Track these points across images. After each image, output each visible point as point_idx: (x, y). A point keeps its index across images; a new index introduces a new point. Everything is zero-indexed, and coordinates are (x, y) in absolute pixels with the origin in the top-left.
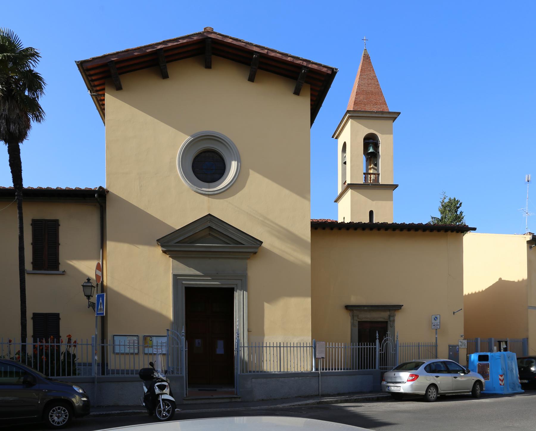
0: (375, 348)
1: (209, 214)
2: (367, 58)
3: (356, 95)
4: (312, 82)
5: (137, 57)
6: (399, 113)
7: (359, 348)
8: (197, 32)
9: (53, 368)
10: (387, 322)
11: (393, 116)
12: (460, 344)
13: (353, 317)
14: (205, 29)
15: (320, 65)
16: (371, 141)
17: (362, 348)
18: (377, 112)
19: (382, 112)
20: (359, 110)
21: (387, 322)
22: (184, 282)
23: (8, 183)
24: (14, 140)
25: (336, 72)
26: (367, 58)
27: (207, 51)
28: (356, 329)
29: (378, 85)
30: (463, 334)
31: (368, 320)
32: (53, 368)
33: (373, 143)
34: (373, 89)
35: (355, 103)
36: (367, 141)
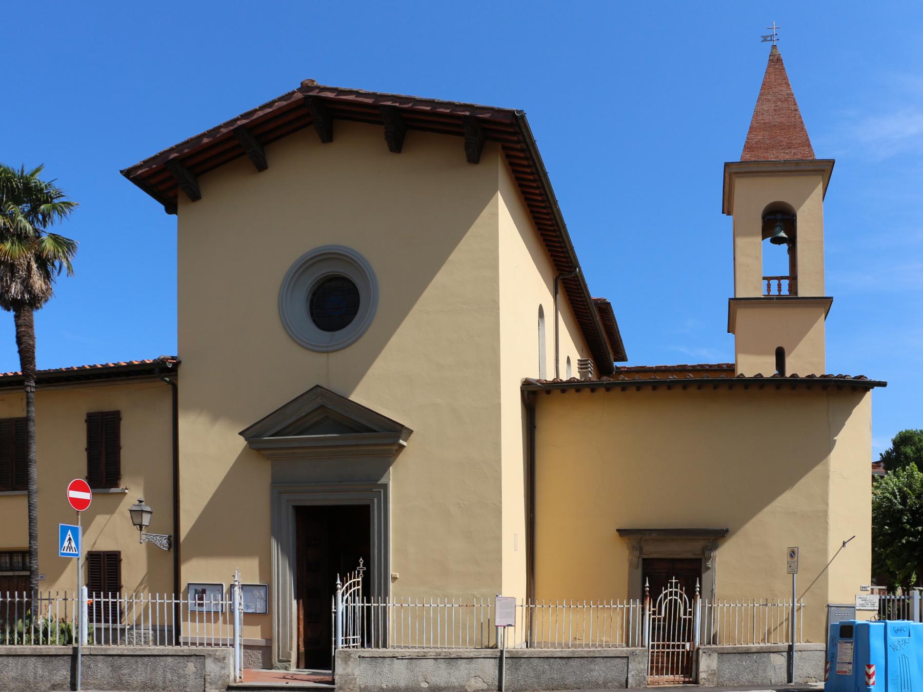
0: (91, 620)
1: (317, 386)
2: (776, 61)
3: (750, 132)
5: (210, 147)
8: (371, 91)
10: (701, 560)
12: (859, 602)
13: (632, 548)
14: (302, 83)
15: (357, 93)
16: (779, 216)
18: (786, 162)
19: (797, 163)
20: (753, 159)
21: (701, 560)
22: (376, 500)
23: (11, 365)
24: (24, 306)
26: (776, 61)
27: (316, 116)
29: (796, 110)
31: (662, 556)
35: (748, 147)
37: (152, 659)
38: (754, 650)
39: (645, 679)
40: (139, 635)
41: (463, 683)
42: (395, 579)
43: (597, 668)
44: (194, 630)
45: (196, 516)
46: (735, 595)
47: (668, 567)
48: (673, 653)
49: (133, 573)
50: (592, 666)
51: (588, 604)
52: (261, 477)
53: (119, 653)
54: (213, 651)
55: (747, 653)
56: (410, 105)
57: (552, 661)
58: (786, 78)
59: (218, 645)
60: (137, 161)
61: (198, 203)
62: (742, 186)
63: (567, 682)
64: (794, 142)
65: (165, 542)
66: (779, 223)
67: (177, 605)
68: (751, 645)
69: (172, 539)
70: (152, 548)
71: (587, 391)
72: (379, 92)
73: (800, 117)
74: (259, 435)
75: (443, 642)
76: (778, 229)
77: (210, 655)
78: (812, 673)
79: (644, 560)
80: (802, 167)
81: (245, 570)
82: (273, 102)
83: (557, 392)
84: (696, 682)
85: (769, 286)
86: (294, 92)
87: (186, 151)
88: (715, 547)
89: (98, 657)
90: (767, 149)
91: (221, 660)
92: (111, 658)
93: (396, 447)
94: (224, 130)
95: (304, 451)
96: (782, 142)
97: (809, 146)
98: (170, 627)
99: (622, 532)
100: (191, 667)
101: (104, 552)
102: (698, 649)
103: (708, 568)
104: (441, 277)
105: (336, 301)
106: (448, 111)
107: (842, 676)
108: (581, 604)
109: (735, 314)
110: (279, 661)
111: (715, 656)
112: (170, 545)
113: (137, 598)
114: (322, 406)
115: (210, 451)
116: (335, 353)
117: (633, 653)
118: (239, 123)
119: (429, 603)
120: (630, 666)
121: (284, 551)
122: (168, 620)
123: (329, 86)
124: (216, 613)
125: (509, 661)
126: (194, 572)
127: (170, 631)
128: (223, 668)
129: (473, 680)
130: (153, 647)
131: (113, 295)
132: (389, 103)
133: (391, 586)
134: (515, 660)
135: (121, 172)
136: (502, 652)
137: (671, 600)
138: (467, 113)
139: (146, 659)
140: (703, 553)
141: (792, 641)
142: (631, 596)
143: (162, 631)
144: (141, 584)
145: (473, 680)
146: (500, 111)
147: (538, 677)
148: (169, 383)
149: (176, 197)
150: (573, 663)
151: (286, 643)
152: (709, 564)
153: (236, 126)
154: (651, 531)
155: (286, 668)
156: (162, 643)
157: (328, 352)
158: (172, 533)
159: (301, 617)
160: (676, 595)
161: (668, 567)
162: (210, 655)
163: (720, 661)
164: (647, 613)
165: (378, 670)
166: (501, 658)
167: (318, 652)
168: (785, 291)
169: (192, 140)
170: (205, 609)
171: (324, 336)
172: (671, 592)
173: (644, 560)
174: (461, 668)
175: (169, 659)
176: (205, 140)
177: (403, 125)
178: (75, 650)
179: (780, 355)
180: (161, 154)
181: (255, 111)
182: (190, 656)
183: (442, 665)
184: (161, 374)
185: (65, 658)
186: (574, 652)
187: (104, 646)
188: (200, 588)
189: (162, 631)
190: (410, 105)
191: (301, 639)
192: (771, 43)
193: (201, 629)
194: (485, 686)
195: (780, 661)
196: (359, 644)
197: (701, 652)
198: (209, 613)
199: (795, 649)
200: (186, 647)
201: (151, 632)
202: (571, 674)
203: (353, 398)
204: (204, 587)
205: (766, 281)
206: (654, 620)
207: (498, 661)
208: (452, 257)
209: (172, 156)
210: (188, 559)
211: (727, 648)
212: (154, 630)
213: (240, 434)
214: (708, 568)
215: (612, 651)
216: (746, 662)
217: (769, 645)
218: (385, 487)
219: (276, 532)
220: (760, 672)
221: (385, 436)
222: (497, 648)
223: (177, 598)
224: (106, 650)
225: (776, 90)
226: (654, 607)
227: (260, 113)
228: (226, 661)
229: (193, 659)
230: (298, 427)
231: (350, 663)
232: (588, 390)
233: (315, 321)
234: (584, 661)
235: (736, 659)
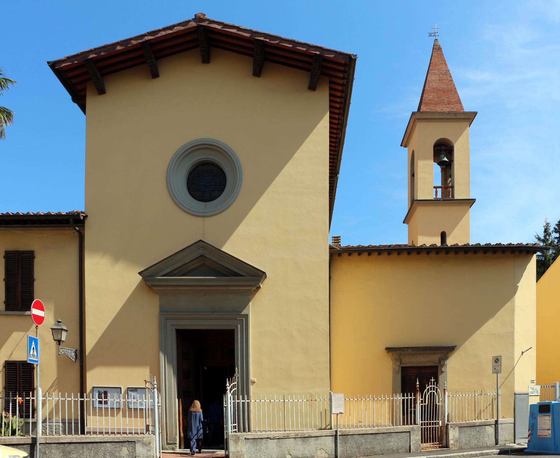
1: (201, 241)
2: (437, 49)
4: (328, 74)
5: (121, 53)
6: (475, 113)
7: (403, 400)
8: (248, 28)
9: (396, 420)
10: (437, 367)
11: (470, 117)
14: (195, 15)
15: (238, 28)
16: (443, 148)
17: (407, 400)
18: (449, 113)
19: (455, 114)
20: (428, 110)
21: (437, 367)
22: (239, 326)
25: (355, 60)
26: (437, 49)
27: (203, 42)
28: (399, 376)
29: (452, 81)
30: (534, 378)
32: (396, 420)
33: (445, 150)
34: (445, 86)
36: (439, 148)
37: (95, 445)
38: (478, 424)
39: (420, 446)
40: (51, 428)
41: (313, 454)
42: (253, 382)
43: (392, 440)
44: (107, 421)
45: (99, 335)
46: (458, 391)
47: (417, 373)
48: (433, 428)
49: (43, 380)
50: (390, 439)
51: (384, 397)
52: (151, 307)
53: (69, 441)
54: (141, 438)
55: (474, 426)
56: (277, 42)
57: (366, 436)
58: (444, 60)
59: (126, 433)
60: (62, 57)
61: (103, 97)
62: (420, 127)
63: (376, 450)
64: (451, 100)
65: (73, 354)
66: (443, 152)
67: (82, 402)
68: (477, 421)
69: (78, 352)
70: (61, 360)
71: (376, 254)
72: (255, 29)
73: (454, 85)
74: (153, 275)
75: (297, 427)
76: (443, 156)
77: (139, 441)
78: (508, 438)
79: (402, 367)
80: (458, 117)
81: (138, 376)
82: (174, 26)
83: (345, 255)
84: (447, 446)
85: (436, 192)
86: (189, 21)
87: (103, 54)
88: (446, 358)
89: (52, 445)
90: (436, 104)
91: (147, 444)
92: (62, 446)
93: (255, 288)
94: (134, 42)
95: (162, 288)
96: (444, 100)
97: (460, 103)
98: (76, 420)
99: (389, 350)
100: (125, 450)
101: (20, 362)
102: (447, 425)
103: (442, 372)
104: (288, 169)
105: (208, 179)
106: (305, 49)
107: (543, 439)
108: (381, 397)
109: (415, 210)
110: (168, 444)
111: (457, 428)
112: (76, 357)
113: (46, 397)
114: (202, 255)
115: (111, 285)
116: (209, 218)
117: (413, 429)
118: (147, 38)
119: (264, 398)
120: (411, 438)
121: (169, 361)
122: (75, 414)
123: (216, 20)
124: (118, 409)
125: (341, 437)
126: (96, 378)
127: (76, 423)
128: (149, 450)
129: (319, 451)
130: (62, 436)
131: (40, 161)
132: (262, 39)
133: (252, 388)
134: (344, 437)
135: (48, 63)
136: (336, 431)
137: (431, 393)
138: (318, 53)
139: (90, 445)
140: (440, 362)
141: (498, 419)
142: (394, 392)
143: (70, 423)
144: (51, 387)
145: (319, 451)
146: (341, 54)
147: (358, 448)
148: (78, 231)
149: (85, 90)
150: (379, 437)
151: (172, 430)
152: (443, 369)
153: (144, 40)
154: (408, 348)
155: (173, 449)
156: (70, 433)
157: (204, 217)
158: (78, 348)
159: (181, 411)
160: (434, 390)
161: (417, 373)
162: (139, 441)
163: (460, 433)
164: (419, 402)
165: (258, 447)
166: (336, 436)
167: (215, 437)
168: (439, 196)
169: (108, 46)
170: (109, 406)
171: (199, 205)
172: (431, 388)
173: (402, 367)
174: (312, 444)
175: (108, 444)
176: (119, 48)
177: (266, 56)
178: (34, 440)
179: (443, 236)
180: (82, 53)
181: (159, 31)
182: (124, 442)
183: (299, 442)
184: (71, 224)
185: (26, 446)
186: (378, 430)
187: (56, 436)
188: (102, 390)
189: (70, 423)
190: (277, 42)
191: (181, 428)
192: (434, 38)
193: (107, 421)
194: (327, 456)
195: (490, 430)
196: (237, 430)
197: (449, 426)
198: (112, 409)
199: (499, 422)
200: (107, 435)
201: (61, 424)
202: (378, 444)
203: (224, 249)
204: (106, 390)
205: (435, 189)
206: (422, 406)
207: (334, 438)
208: (296, 155)
209: (91, 56)
210: (92, 367)
211: (463, 424)
212: (64, 423)
213: (140, 273)
214: (442, 372)
215: (383, 429)
216: (473, 432)
217: (480, 421)
218: (247, 316)
219: (163, 348)
220: (481, 438)
221: (248, 278)
222: (331, 429)
223: (82, 396)
224: (58, 439)
225: (439, 67)
226: (422, 398)
227: (163, 33)
228: (151, 445)
229: (126, 444)
230: (183, 271)
231: (239, 443)
232: (386, 253)
233: (190, 194)
234: (385, 435)
235: (468, 431)
